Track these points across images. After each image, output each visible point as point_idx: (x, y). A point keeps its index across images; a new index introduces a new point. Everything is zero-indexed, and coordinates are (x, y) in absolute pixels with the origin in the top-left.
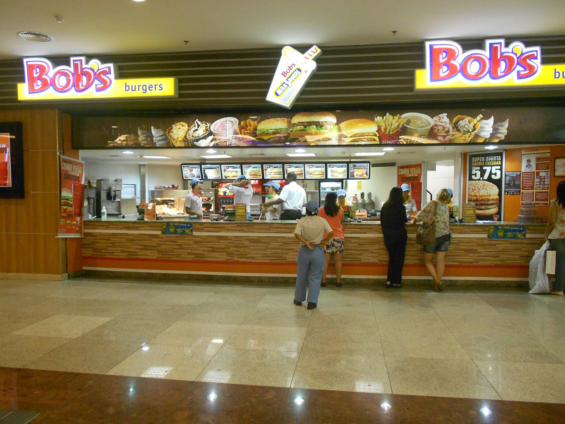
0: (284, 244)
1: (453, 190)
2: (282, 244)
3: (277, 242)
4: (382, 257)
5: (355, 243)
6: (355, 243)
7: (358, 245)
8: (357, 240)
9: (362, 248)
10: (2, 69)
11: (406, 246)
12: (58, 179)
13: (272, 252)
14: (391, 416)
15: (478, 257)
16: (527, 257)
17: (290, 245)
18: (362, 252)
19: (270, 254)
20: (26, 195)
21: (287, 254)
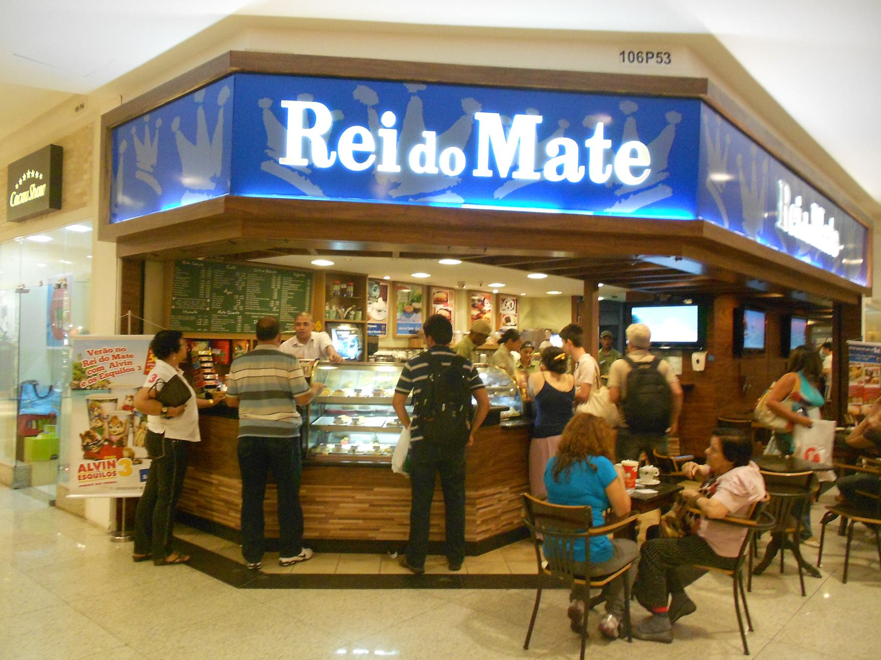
0: (372, 505)
1: (486, 343)
2: (367, 505)
3: (355, 503)
4: (388, 533)
5: (361, 502)
6: (361, 502)
7: (370, 506)
8: (368, 495)
9: (379, 514)
10: (879, 312)
11: (444, 511)
12: (188, 91)
13: (342, 526)
14: (676, 573)
15: (341, 532)
16: (149, 533)
17: (384, 508)
18: (379, 523)
19: (336, 529)
20: (63, 204)
21: (378, 530)
